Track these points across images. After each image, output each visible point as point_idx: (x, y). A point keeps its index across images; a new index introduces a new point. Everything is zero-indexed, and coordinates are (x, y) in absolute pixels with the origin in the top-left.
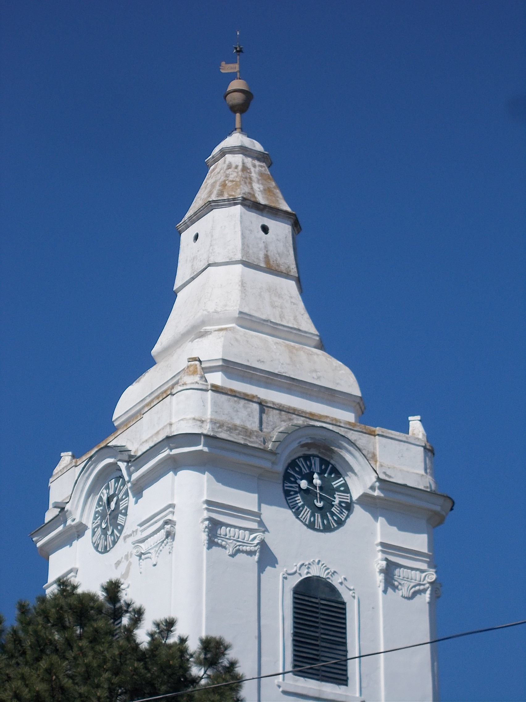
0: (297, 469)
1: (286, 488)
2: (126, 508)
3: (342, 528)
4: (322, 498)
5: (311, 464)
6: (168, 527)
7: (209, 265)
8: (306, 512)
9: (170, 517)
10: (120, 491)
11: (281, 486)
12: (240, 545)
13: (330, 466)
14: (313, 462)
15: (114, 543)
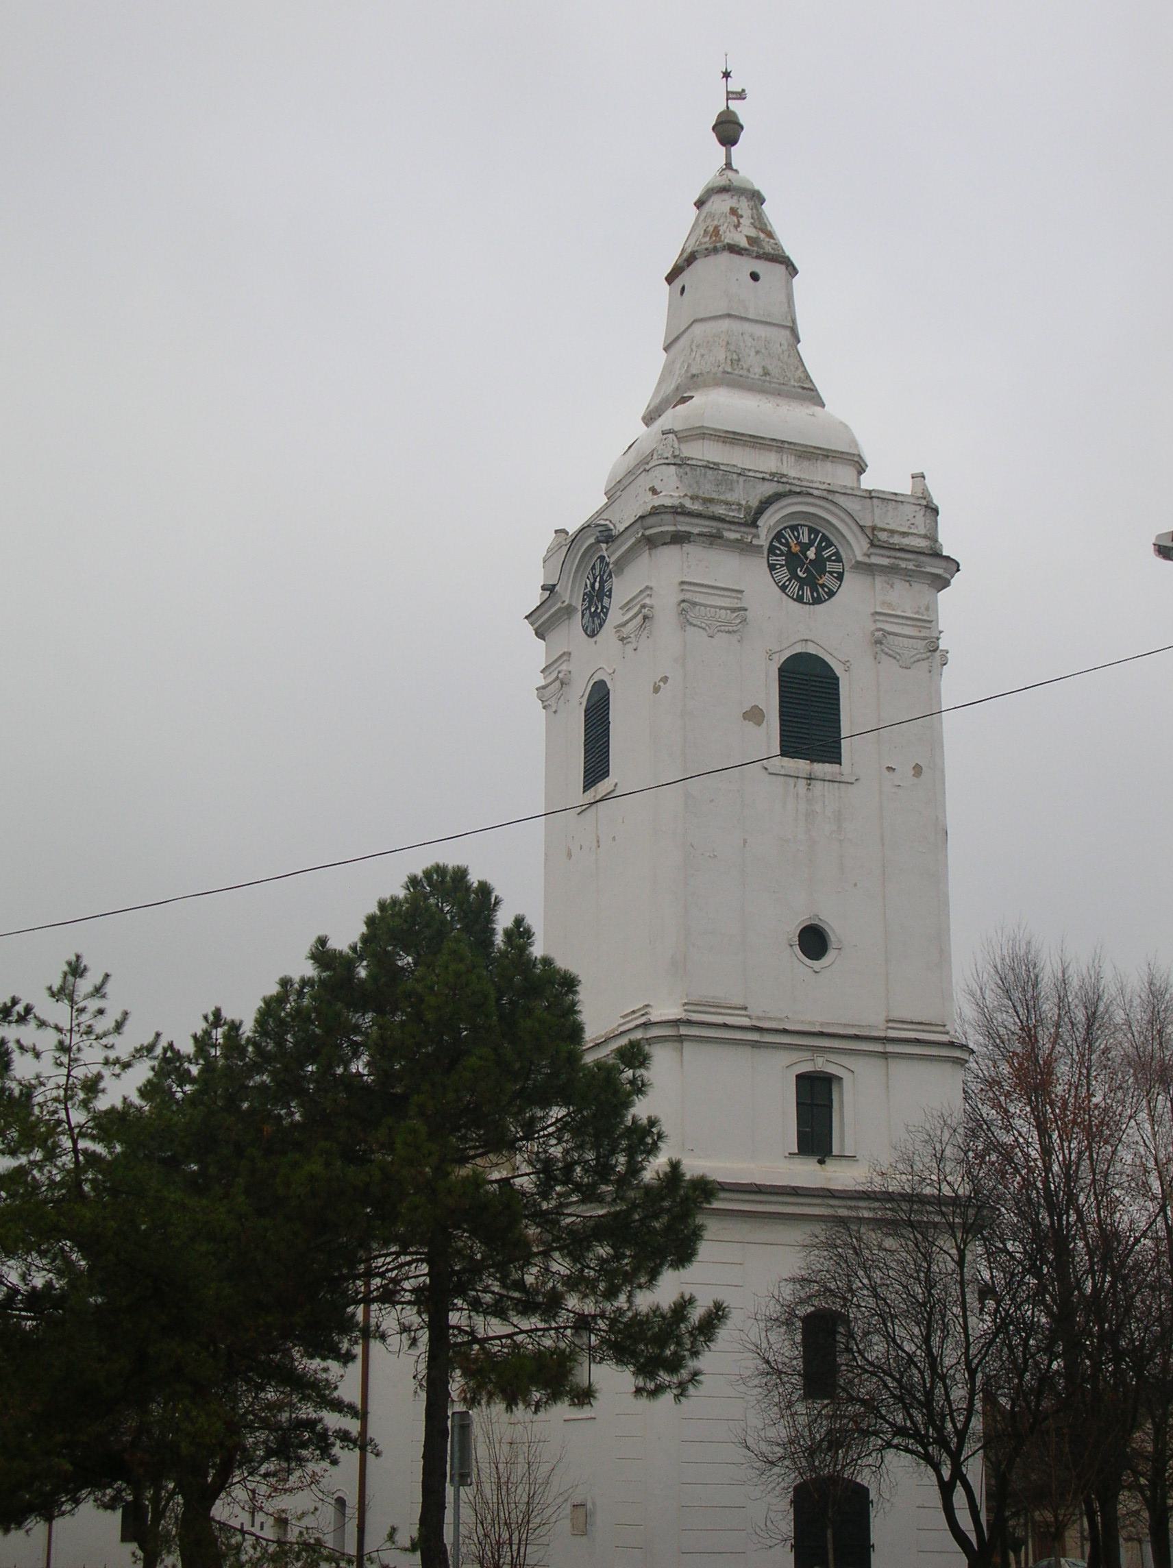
0: (783, 541)
1: (771, 562)
2: (610, 590)
3: (833, 599)
4: (807, 570)
5: (799, 534)
6: (645, 611)
7: (695, 321)
8: (784, 574)
9: (647, 601)
10: (604, 572)
11: (765, 560)
12: (720, 626)
13: (821, 534)
14: (801, 532)
15: (601, 626)
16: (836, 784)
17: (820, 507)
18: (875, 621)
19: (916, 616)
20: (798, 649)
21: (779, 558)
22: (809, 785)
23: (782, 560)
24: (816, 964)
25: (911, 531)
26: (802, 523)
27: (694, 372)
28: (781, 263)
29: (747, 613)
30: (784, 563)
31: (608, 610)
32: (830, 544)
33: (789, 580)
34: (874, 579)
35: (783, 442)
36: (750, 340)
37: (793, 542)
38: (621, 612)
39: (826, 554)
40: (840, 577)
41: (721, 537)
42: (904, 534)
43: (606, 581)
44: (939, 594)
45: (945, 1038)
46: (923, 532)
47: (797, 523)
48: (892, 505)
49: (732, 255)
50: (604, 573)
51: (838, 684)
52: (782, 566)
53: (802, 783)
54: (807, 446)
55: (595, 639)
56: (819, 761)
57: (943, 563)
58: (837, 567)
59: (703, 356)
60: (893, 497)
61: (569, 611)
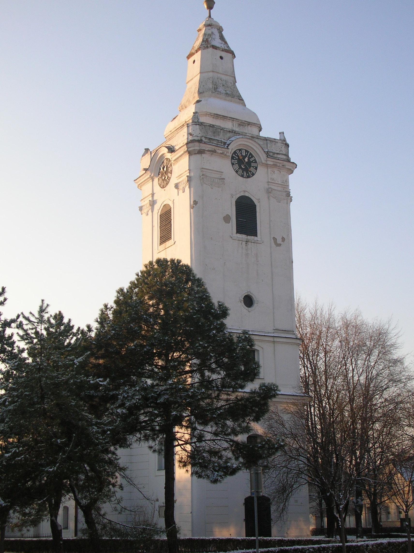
2: (171, 171)
8: (237, 167)
10: (168, 164)
15: (167, 184)
16: (256, 244)
17: (250, 143)
18: (268, 185)
19: (282, 184)
20: (242, 194)
21: (235, 161)
22: (246, 244)
23: (236, 161)
24: (250, 309)
25: (280, 153)
26: (243, 148)
27: (201, 92)
28: (230, 53)
29: (224, 180)
30: (237, 162)
31: (170, 178)
32: (253, 156)
33: (239, 169)
34: (268, 168)
35: (234, 119)
36: (220, 81)
37: (240, 155)
38: (177, 179)
39: (251, 160)
40: (256, 169)
41: (216, 152)
42: (278, 154)
43: (169, 167)
44: (289, 176)
45: (294, 337)
46: (284, 153)
47: (241, 148)
48: (273, 143)
49: (214, 49)
50: (168, 165)
51: (256, 207)
52: (236, 164)
53: (244, 243)
54: (242, 121)
55: (164, 189)
56: (249, 235)
57: (292, 165)
58: (255, 165)
59: (203, 86)
60: (274, 140)
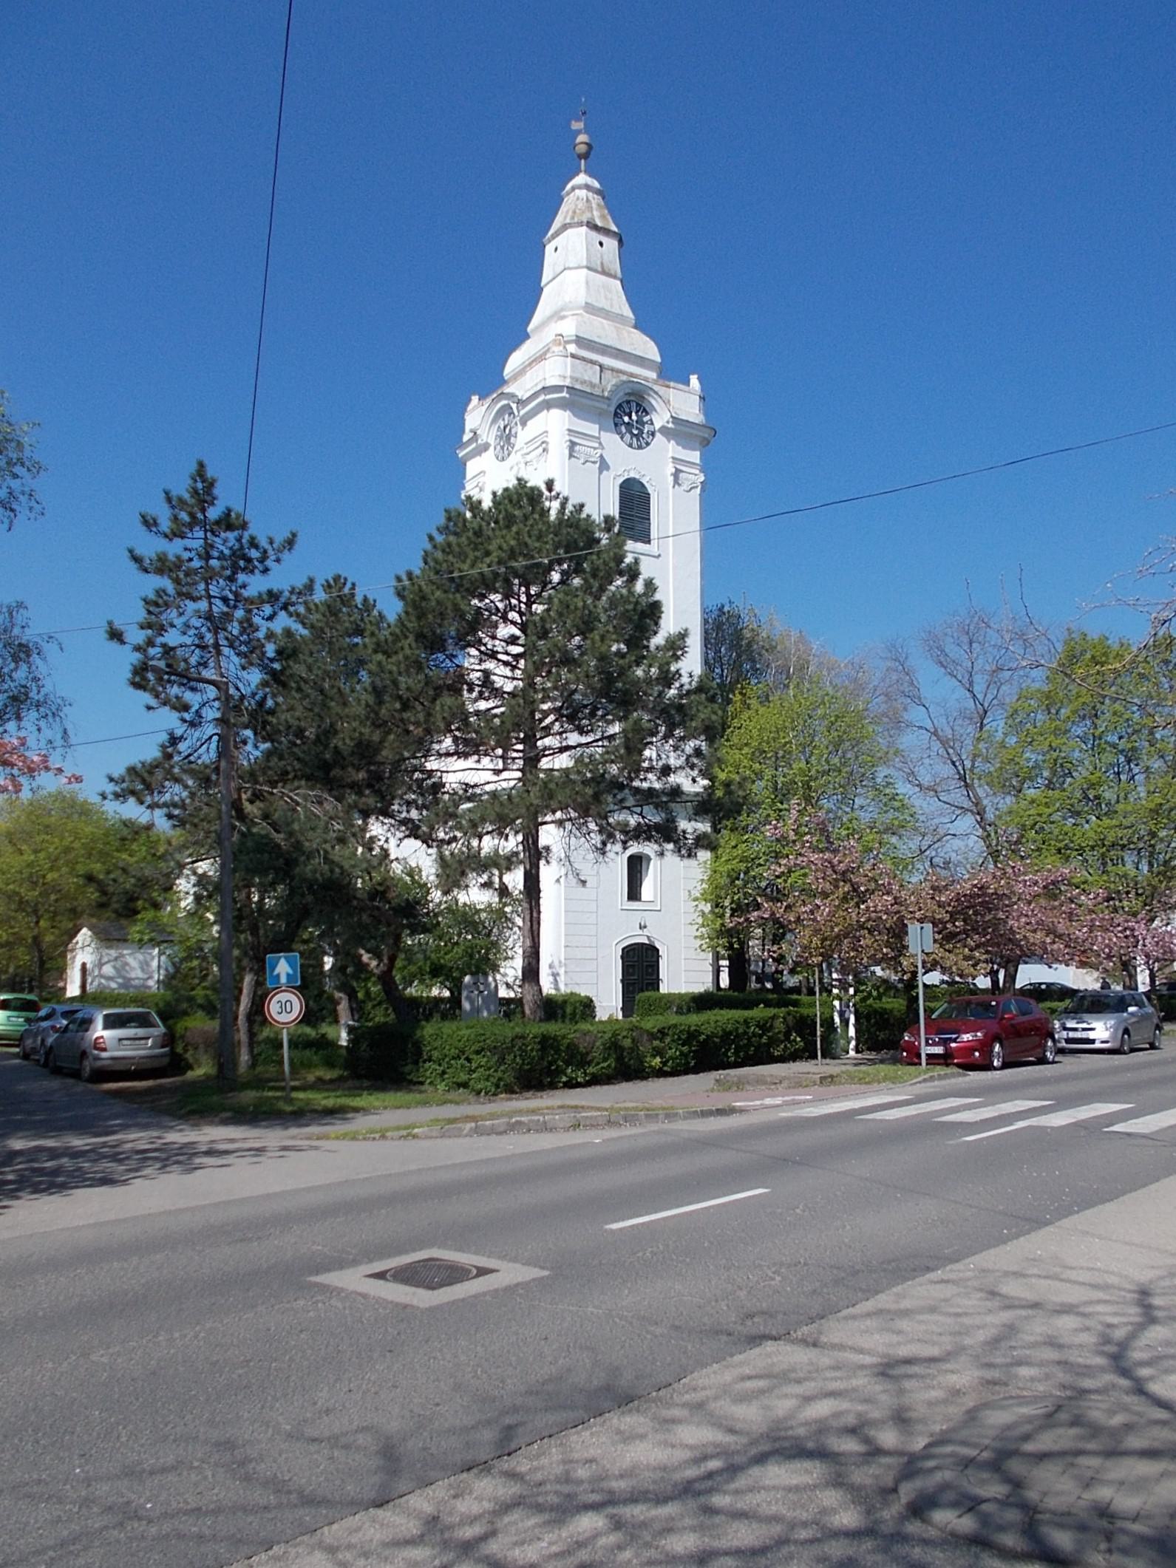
15: (509, 455)
61: (486, 447)
